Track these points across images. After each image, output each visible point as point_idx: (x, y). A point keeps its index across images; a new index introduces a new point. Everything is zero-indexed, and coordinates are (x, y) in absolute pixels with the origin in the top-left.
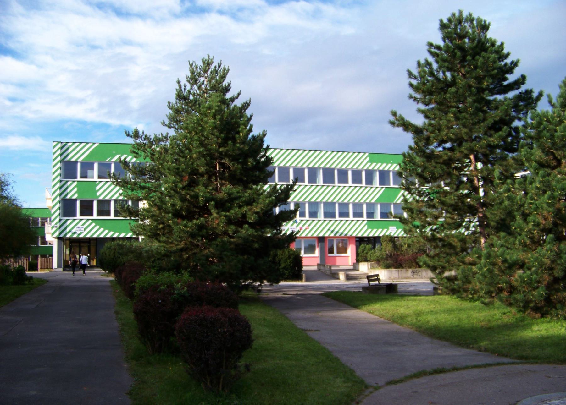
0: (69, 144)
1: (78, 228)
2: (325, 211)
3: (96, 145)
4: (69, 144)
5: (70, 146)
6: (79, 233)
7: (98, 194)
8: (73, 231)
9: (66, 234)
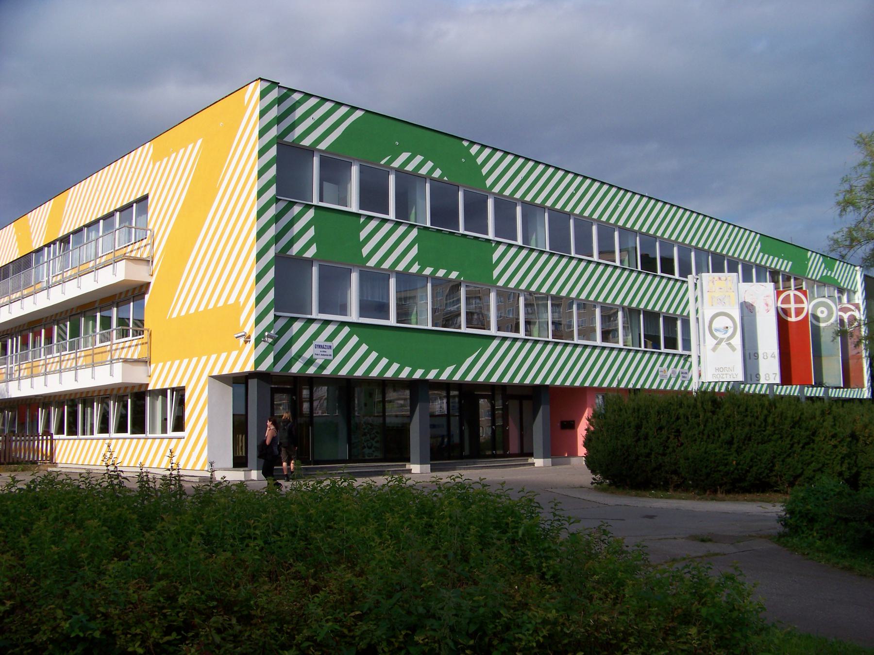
0: (297, 97)
1: (320, 346)
3: (358, 114)
4: (297, 97)
5: (299, 103)
6: (320, 361)
7: (365, 251)
8: (307, 355)
9: (290, 365)
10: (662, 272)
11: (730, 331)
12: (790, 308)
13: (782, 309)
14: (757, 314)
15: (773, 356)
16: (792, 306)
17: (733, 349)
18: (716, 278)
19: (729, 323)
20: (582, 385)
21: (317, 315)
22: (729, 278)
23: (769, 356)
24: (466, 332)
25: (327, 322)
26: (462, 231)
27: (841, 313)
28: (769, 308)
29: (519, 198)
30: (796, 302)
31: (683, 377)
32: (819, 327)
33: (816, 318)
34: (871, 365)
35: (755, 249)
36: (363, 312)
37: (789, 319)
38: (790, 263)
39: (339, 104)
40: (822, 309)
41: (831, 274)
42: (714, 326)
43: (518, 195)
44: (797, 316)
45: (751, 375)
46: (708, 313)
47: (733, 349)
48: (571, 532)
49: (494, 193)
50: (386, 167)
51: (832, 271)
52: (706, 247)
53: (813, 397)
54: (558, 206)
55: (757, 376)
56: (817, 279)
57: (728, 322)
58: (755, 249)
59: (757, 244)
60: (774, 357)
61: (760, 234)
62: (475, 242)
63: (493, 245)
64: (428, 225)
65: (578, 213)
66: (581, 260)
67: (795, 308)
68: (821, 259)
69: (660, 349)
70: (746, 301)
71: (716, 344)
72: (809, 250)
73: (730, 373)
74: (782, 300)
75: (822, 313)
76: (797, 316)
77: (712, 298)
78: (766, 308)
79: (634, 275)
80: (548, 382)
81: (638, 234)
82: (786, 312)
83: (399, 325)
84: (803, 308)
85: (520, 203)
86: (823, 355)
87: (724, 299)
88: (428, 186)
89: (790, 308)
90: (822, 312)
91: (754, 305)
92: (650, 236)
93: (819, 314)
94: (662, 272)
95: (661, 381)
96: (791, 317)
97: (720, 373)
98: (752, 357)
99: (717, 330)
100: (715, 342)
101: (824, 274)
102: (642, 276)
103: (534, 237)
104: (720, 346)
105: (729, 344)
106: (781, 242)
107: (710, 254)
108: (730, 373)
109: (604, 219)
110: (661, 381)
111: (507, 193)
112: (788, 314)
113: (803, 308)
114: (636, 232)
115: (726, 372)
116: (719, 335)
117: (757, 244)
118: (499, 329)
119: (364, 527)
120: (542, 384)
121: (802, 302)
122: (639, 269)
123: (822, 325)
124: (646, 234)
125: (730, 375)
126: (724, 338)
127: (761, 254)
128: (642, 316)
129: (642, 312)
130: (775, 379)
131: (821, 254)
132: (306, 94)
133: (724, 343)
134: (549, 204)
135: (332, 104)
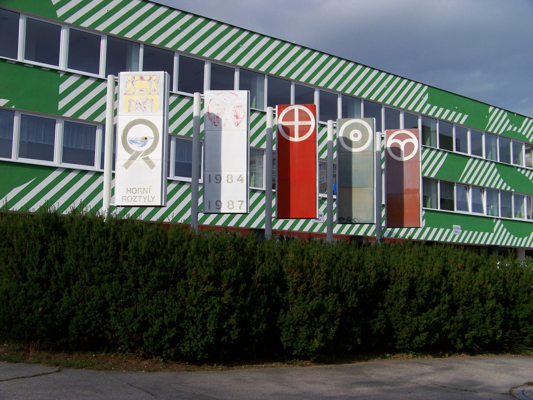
2: (177, 161)
10: (179, 90)
11: (150, 143)
12: (293, 126)
13: (283, 127)
14: (223, 128)
15: (240, 179)
16: (296, 123)
17: (151, 165)
18: (137, 78)
19: (150, 133)
20: (418, 239)
21: (17, 159)
22: (154, 78)
23: (235, 179)
24: (457, 212)
25: (69, 171)
26: (20, 58)
27: (397, 141)
28: (239, 120)
29: (294, 79)
30: (300, 119)
31: (456, 232)
32: (350, 153)
33: (349, 143)
35: (421, 99)
36: (473, 211)
37: (291, 139)
38: (466, 117)
39: (232, 27)
40: (360, 136)
41: (517, 130)
42: (130, 136)
43: (340, 89)
45: (210, 202)
46: (122, 121)
47: (151, 165)
49: (320, 87)
50: (234, 66)
51: (519, 127)
52: (495, 132)
53: (361, 237)
54: (373, 98)
55: (218, 203)
56: (500, 133)
57: (148, 132)
58: (421, 99)
59: (424, 95)
61: (428, 86)
62: (36, 71)
63: (61, 75)
64: (498, 161)
65: (331, 88)
66: (475, 159)
68: (506, 115)
69: (453, 210)
70: (210, 112)
71: (130, 159)
72: (491, 106)
73: (145, 195)
74: (308, 131)
75: (355, 136)
77: (130, 102)
78: (236, 120)
79: (433, 152)
80: (493, 243)
81: (438, 121)
82: (288, 130)
83: (488, 216)
84: (310, 126)
85: (341, 95)
86: (353, 186)
87: (144, 103)
88: (266, 80)
89: (293, 126)
90: (356, 135)
91: (220, 116)
92: (449, 122)
93: (352, 138)
94: (179, 90)
95: (454, 236)
96: (293, 136)
97: (132, 195)
98: (213, 179)
99: (132, 142)
100: (130, 156)
101: (509, 129)
102: (440, 154)
103: (429, 139)
104: (135, 162)
105: (147, 159)
106: (476, 102)
107: (498, 137)
108: (145, 195)
109: (410, 108)
110: (454, 236)
111: (331, 87)
112: (290, 133)
113: (310, 126)
114: (436, 119)
115: (140, 194)
116: (134, 147)
117: (424, 95)
118: (64, 160)
119: (514, 311)
120: (259, 228)
122: (438, 148)
123: (354, 150)
124: (445, 121)
126: (141, 152)
127: (428, 106)
128: (439, 184)
129: (439, 181)
130: (240, 208)
131: (505, 110)
132: (416, 82)
133: (140, 158)
134: (365, 96)
135: (378, 72)
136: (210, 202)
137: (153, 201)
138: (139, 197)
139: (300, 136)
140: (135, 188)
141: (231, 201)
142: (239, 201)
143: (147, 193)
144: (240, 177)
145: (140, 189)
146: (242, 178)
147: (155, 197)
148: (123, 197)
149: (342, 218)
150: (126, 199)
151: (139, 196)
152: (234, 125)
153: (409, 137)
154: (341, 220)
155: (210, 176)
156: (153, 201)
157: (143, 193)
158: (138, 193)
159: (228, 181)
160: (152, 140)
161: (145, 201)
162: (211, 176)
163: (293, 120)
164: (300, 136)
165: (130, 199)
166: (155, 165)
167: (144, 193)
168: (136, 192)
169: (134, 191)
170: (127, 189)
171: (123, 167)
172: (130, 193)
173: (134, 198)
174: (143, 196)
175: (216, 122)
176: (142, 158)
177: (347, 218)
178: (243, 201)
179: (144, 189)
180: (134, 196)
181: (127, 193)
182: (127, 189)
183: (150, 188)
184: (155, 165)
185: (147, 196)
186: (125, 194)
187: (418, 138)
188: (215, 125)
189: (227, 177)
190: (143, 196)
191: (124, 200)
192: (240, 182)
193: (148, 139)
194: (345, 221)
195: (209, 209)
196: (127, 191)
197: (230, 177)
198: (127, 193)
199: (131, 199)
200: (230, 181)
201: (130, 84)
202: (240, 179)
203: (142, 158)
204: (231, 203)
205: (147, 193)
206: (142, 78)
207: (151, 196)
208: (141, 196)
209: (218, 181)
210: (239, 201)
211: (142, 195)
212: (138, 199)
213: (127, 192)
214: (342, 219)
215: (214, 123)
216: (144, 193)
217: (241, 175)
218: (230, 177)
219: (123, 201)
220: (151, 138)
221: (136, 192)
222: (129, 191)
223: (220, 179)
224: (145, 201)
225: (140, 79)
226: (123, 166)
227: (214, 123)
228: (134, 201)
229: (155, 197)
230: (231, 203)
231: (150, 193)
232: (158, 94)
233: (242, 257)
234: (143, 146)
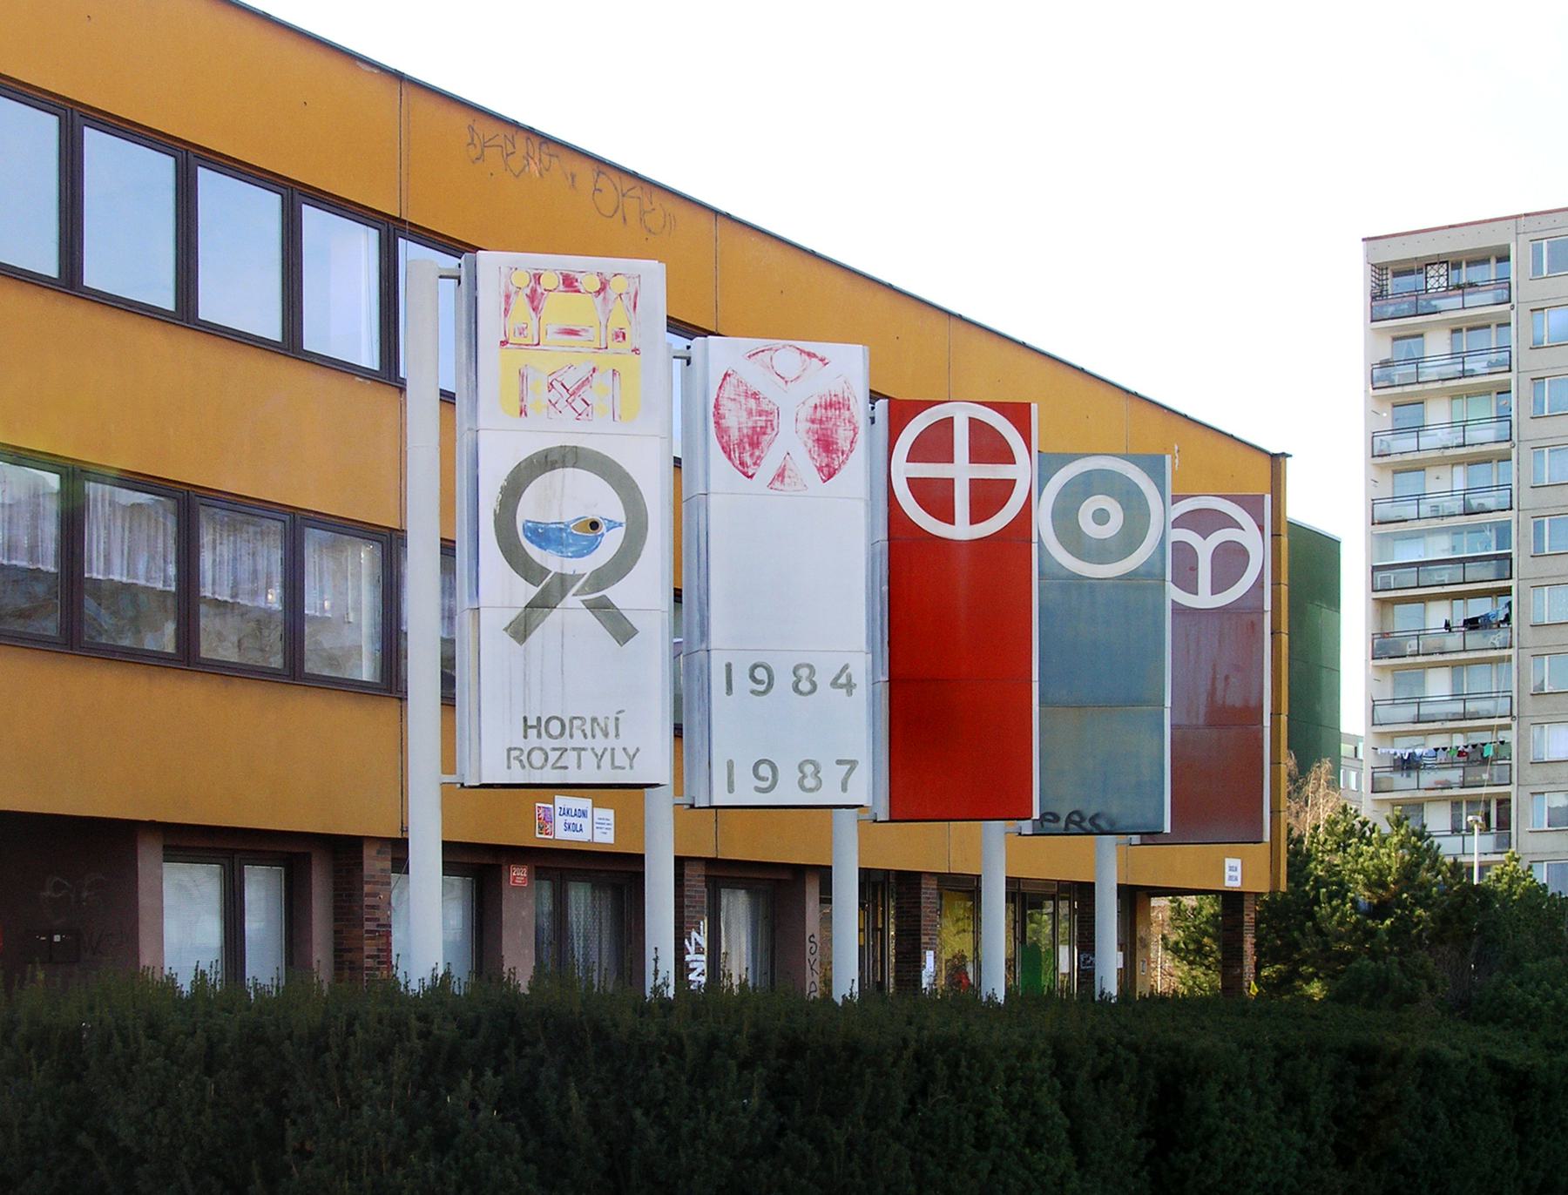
11: (611, 543)
17: (621, 629)
19: (609, 506)
23: (823, 680)
30: (976, 456)
34: (1289, 592)
40: (1098, 501)
42: (529, 509)
44: (977, 517)
45: (730, 765)
47: (621, 629)
48: (1462, 624)
60: (850, 686)
67: (951, 460)
73: (600, 743)
74: (1002, 503)
76: (977, 517)
84: (1011, 484)
99: (542, 535)
104: (555, 616)
105: (601, 608)
113: (1011, 484)
115: (578, 741)
116: (551, 561)
121: (1007, 457)
125: (600, 758)
130: (844, 789)
133: (572, 601)
136: (730, 765)
137: (631, 767)
138: (575, 753)
139: (975, 519)
140: (557, 718)
141: (812, 762)
142: (839, 762)
143: (606, 735)
144: (842, 671)
145: (577, 723)
146: (849, 678)
147: (638, 750)
148: (509, 750)
149: (1051, 814)
150: (524, 758)
151: (574, 749)
152: (817, 476)
153: (1231, 523)
154: (1045, 823)
155: (729, 666)
156: (631, 767)
157: (589, 734)
158: (571, 736)
159: (796, 689)
160: (620, 533)
161: (599, 767)
162: (733, 668)
163: (950, 459)
164: (975, 519)
165: (537, 758)
166: (634, 632)
167: (593, 736)
168: (562, 734)
169: (555, 727)
170: (525, 719)
171: (506, 635)
172: (539, 735)
173: (553, 756)
174: (593, 749)
175: (748, 460)
176: (583, 601)
177: (1070, 815)
178: (853, 764)
179: (594, 720)
180: (554, 749)
181: (525, 737)
182: (525, 719)
183: (617, 719)
184: (634, 632)
185: (605, 749)
186: (518, 741)
187: (1261, 529)
188: (745, 474)
189: (794, 673)
190: (593, 749)
191: (515, 764)
192: (844, 690)
193: (603, 529)
194: (1062, 824)
195: (731, 789)
196: (526, 727)
197: (804, 672)
198: (525, 737)
199: (543, 756)
200: (805, 686)
201: (521, 304)
202: (843, 680)
203: (583, 601)
204: (809, 769)
205: (606, 735)
206: (569, 283)
207: (624, 749)
208: (584, 749)
209: (762, 688)
210: (839, 762)
211: (589, 743)
212: (571, 758)
213: (525, 731)
214: (1051, 818)
215: (742, 463)
216: (593, 736)
217: (846, 667)
218: (804, 672)
219: (509, 767)
220: (613, 525)
221: (562, 734)
222: (531, 727)
223: (767, 681)
224: (599, 767)
225: (562, 287)
226: (506, 629)
227: (742, 463)
228: (554, 767)
229: (638, 750)
230: (809, 769)
231: (617, 735)
232: (635, 350)
233: (1561, 987)
234: (582, 555)
